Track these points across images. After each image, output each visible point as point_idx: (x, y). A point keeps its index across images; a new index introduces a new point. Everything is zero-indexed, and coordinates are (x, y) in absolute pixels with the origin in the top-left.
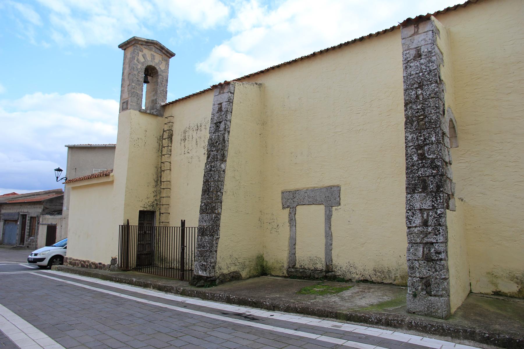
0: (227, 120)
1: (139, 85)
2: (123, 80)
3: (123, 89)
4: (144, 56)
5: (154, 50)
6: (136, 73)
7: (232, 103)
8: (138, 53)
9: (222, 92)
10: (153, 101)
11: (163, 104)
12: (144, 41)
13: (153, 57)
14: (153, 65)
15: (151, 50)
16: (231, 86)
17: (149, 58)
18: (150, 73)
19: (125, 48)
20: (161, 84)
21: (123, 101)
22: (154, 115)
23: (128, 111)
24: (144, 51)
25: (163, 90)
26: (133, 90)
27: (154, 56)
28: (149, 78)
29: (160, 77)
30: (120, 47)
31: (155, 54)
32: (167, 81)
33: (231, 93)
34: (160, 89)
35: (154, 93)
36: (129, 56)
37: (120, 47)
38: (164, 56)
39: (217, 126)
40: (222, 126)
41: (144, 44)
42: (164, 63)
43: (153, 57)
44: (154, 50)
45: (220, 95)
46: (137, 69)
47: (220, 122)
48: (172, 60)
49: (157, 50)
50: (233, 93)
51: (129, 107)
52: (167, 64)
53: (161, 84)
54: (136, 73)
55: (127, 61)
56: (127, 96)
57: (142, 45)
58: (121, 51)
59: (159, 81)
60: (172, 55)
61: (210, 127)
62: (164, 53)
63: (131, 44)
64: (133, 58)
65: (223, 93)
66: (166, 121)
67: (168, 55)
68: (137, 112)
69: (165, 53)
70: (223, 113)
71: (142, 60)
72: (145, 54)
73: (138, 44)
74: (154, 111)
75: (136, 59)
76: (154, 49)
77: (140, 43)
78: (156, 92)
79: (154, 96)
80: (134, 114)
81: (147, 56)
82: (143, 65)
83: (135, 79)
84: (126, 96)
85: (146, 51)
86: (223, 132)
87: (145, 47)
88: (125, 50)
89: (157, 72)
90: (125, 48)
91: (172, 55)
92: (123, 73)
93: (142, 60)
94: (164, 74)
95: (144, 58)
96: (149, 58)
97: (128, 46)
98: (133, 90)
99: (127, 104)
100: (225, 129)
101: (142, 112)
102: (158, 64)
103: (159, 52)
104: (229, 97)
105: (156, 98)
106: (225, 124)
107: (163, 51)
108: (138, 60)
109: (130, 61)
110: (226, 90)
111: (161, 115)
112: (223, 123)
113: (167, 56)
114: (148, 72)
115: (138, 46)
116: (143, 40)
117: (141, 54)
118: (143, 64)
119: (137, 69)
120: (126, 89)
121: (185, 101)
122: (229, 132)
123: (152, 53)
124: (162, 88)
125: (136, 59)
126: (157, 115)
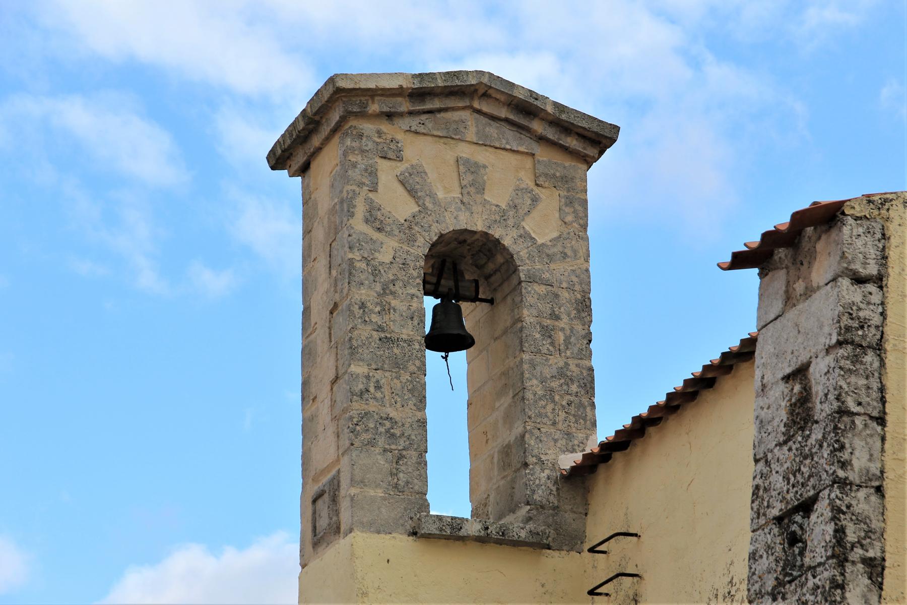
0: (843, 484)
1: (398, 365)
2: (308, 354)
3: (419, 415)
4: (411, 184)
5: (471, 135)
6: (366, 294)
7: (879, 348)
8: (372, 173)
9: (800, 287)
10: (506, 451)
11: (569, 461)
12: (399, 92)
13: (472, 177)
14: (479, 226)
15: (452, 136)
16: (849, 229)
17: (444, 187)
18: (466, 277)
19: (299, 159)
20: (548, 333)
21: (315, 489)
22: (517, 544)
23: (342, 544)
24: (407, 153)
25: (561, 373)
26: (358, 406)
27: (474, 168)
28: (472, 316)
29: (533, 293)
30: (279, 159)
31: (483, 156)
32: (584, 307)
33: (859, 280)
34: (542, 370)
35: (506, 401)
36: (325, 201)
37: (279, 159)
38: (543, 154)
39: (793, 540)
40: (819, 529)
41: (405, 105)
42: (551, 199)
43: (472, 177)
44: (471, 134)
45: (791, 314)
46: (375, 273)
47: (806, 507)
48: (602, 176)
49: (493, 130)
50: (879, 280)
51: (345, 517)
52: (576, 203)
53: (548, 333)
54: (366, 294)
55: (319, 233)
56: (332, 453)
57: (390, 116)
58: (290, 184)
59: (528, 316)
60: (596, 139)
61: (753, 556)
62: (541, 139)
63: (325, 130)
64: (345, 207)
65: (809, 291)
66: (602, 568)
67: (572, 142)
68: (399, 544)
69: (551, 133)
70: (817, 434)
71: (399, 206)
72: (417, 171)
73: (362, 114)
74: (517, 524)
75: (360, 210)
76: (472, 125)
77: (374, 107)
78: (520, 396)
79: (509, 419)
80: (376, 551)
81: (432, 176)
82: (411, 240)
83: (364, 332)
84: (327, 449)
85: (423, 151)
86: (825, 575)
87: (413, 123)
88: (303, 170)
89: (510, 266)
90: (299, 159)
91: (596, 139)
92: (306, 312)
93: (399, 206)
94: (560, 270)
95: (412, 192)
96: (444, 187)
97: (316, 141)
98: (358, 406)
99: (334, 500)
100: (840, 552)
101: (428, 537)
102: (513, 211)
103: (510, 138)
104: (849, 310)
105: (518, 429)
106: (837, 512)
107: (538, 127)
108: (374, 218)
109: (335, 230)
110: (822, 269)
111: (571, 541)
112: (822, 508)
113: (565, 149)
114: (457, 274)
115: (368, 127)
116: (394, 84)
117: (387, 173)
118: (408, 229)
119: (375, 273)
120: (324, 410)
121: (672, 423)
122: (875, 569)
123: (464, 151)
124: (557, 361)
125: (360, 210)
126: (538, 544)
